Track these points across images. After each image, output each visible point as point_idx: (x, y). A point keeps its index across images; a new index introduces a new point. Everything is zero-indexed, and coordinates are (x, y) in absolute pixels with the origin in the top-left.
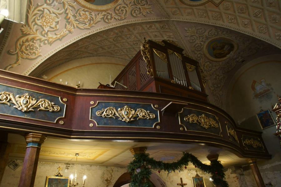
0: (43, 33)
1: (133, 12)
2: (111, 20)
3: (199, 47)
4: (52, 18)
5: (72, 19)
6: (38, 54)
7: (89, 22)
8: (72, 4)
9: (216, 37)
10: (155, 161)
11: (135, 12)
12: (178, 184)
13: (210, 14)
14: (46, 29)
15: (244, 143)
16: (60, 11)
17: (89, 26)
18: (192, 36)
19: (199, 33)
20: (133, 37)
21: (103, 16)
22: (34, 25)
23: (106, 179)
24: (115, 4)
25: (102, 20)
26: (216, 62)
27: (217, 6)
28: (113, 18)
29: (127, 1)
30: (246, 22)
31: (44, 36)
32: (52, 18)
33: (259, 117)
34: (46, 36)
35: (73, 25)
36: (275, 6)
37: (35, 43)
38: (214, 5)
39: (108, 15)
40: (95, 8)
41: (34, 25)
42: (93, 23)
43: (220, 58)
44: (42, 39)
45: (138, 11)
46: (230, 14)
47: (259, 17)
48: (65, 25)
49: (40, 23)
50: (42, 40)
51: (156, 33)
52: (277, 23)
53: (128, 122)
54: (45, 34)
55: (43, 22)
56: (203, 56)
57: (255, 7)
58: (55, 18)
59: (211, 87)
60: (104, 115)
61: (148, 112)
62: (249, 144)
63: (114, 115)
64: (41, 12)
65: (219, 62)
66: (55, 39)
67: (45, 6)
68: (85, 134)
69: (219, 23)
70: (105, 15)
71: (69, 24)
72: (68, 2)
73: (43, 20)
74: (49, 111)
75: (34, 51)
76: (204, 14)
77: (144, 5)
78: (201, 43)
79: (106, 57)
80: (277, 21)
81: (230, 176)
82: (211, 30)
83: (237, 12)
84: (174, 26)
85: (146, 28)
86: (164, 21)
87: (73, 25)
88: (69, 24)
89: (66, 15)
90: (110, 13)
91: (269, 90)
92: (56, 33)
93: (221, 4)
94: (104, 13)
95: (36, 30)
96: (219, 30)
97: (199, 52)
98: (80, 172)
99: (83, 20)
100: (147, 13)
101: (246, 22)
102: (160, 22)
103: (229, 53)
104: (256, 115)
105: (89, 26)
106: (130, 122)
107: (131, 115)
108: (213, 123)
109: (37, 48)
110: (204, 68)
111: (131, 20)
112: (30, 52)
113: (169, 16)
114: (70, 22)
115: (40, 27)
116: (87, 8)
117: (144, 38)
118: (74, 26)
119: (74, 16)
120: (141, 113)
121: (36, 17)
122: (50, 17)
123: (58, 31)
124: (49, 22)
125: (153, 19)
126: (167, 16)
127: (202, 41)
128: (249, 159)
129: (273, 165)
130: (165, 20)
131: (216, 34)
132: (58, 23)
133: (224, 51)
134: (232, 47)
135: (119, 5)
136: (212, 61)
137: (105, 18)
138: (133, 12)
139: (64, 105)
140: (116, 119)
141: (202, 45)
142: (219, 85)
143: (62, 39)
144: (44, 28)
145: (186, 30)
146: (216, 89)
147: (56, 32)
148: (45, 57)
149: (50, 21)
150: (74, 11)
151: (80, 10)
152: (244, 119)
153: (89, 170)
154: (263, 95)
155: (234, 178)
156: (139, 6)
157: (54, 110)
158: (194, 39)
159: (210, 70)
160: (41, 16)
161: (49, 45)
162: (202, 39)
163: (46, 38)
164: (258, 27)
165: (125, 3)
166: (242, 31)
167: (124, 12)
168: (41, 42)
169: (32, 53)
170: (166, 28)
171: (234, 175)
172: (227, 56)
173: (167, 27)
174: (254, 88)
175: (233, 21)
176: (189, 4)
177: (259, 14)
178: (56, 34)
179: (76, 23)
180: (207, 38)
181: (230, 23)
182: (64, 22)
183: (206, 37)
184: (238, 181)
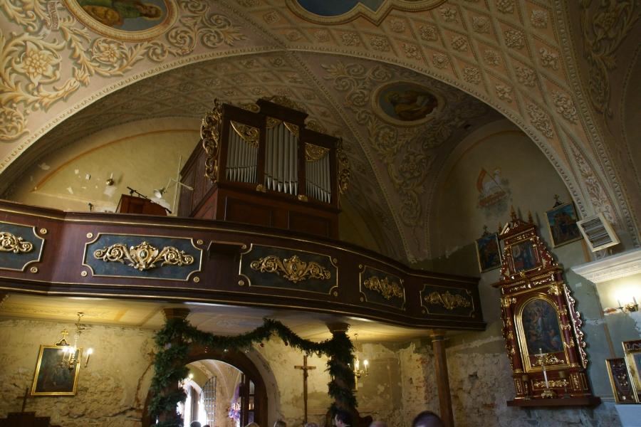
0: (31, 87)
1: (205, 39)
2: (163, 56)
4: (45, 59)
5: (84, 57)
6: (21, 130)
7: (119, 62)
8: (80, 30)
9: (391, 82)
10: (200, 332)
11: (209, 39)
12: (295, 367)
13: (365, 39)
14: (36, 80)
15: (423, 300)
16: (58, 44)
17: (119, 70)
18: (340, 79)
20: (219, 82)
21: (146, 49)
22: (10, 74)
23: (150, 351)
24: (165, 27)
25: (146, 56)
26: (404, 127)
27: (378, 24)
28: (167, 52)
30: (441, 57)
31: (33, 95)
32: (45, 59)
33: (479, 247)
34: (36, 93)
35: (88, 69)
36: (487, 33)
37: (15, 108)
39: (156, 47)
40: (126, 36)
41: (10, 74)
42: (128, 63)
43: (412, 120)
44: (28, 99)
46: (407, 41)
47: (463, 51)
48: (71, 71)
49: (22, 68)
50: (29, 101)
51: (265, 74)
52: (496, 65)
53: (144, 270)
54: (33, 89)
55: (27, 67)
56: (373, 117)
58: (50, 57)
59: (396, 178)
60: (106, 258)
61: (183, 252)
62: (437, 302)
63: (122, 258)
64: (22, 49)
65: (411, 127)
66: (54, 98)
67: (26, 36)
68: (71, 289)
69: (388, 58)
70: (148, 48)
71: (80, 69)
72: (71, 28)
73: (28, 63)
74: (12, 251)
75: (15, 124)
76: (355, 40)
77: (224, 26)
78: (362, 93)
79: (176, 118)
80: (496, 62)
81: (413, 358)
83: (419, 37)
85: (241, 67)
86: (275, 52)
87: (88, 69)
88: (80, 69)
89: (70, 51)
90: (159, 42)
91: (503, 193)
92: (57, 88)
93: (384, 22)
94: (146, 44)
95: (16, 84)
97: (362, 109)
98: (102, 338)
99: (107, 59)
101: (441, 57)
104: (476, 242)
105: (119, 70)
106: (148, 271)
107: (151, 259)
108: (315, 270)
109: (21, 118)
110: (377, 140)
111: (203, 55)
112: (6, 127)
113: (282, 43)
114: (80, 65)
115: (22, 77)
116: (110, 36)
117: (215, 100)
118: (89, 71)
119: (87, 52)
120: (169, 254)
121: (13, 58)
122: (41, 57)
123: (59, 82)
124: (40, 66)
125: (250, 49)
127: (364, 88)
128: (431, 331)
129: (486, 341)
130: (277, 50)
131: (390, 76)
132: (57, 66)
134: (432, 103)
135: (173, 29)
136: (395, 125)
137: (150, 54)
138: (205, 39)
139: (42, 240)
140: (125, 263)
141: (365, 96)
142: (416, 174)
143: (67, 97)
144: (32, 77)
145: (326, 69)
146: (408, 182)
147: (56, 85)
148: (36, 136)
149: (40, 64)
150: (86, 43)
151: (98, 40)
152: (456, 249)
153: (120, 336)
154: (494, 201)
155: (417, 360)
156: (214, 29)
157: (21, 250)
158: (347, 84)
159: (393, 144)
160: (22, 55)
161: (43, 112)
163: (36, 98)
164: (464, 70)
165: (184, 25)
167: (188, 40)
168: (26, 105)
169: (10, 129)
171: (417, 356)
173: (284, 62)
174: (480, 186)
175: (414, 54)
177: (462, 45)
178: (55, 89)
179: (93, 66)
181: (408, 57)
182: (71, 64)
183: (371, 81)
184: (423, 367)
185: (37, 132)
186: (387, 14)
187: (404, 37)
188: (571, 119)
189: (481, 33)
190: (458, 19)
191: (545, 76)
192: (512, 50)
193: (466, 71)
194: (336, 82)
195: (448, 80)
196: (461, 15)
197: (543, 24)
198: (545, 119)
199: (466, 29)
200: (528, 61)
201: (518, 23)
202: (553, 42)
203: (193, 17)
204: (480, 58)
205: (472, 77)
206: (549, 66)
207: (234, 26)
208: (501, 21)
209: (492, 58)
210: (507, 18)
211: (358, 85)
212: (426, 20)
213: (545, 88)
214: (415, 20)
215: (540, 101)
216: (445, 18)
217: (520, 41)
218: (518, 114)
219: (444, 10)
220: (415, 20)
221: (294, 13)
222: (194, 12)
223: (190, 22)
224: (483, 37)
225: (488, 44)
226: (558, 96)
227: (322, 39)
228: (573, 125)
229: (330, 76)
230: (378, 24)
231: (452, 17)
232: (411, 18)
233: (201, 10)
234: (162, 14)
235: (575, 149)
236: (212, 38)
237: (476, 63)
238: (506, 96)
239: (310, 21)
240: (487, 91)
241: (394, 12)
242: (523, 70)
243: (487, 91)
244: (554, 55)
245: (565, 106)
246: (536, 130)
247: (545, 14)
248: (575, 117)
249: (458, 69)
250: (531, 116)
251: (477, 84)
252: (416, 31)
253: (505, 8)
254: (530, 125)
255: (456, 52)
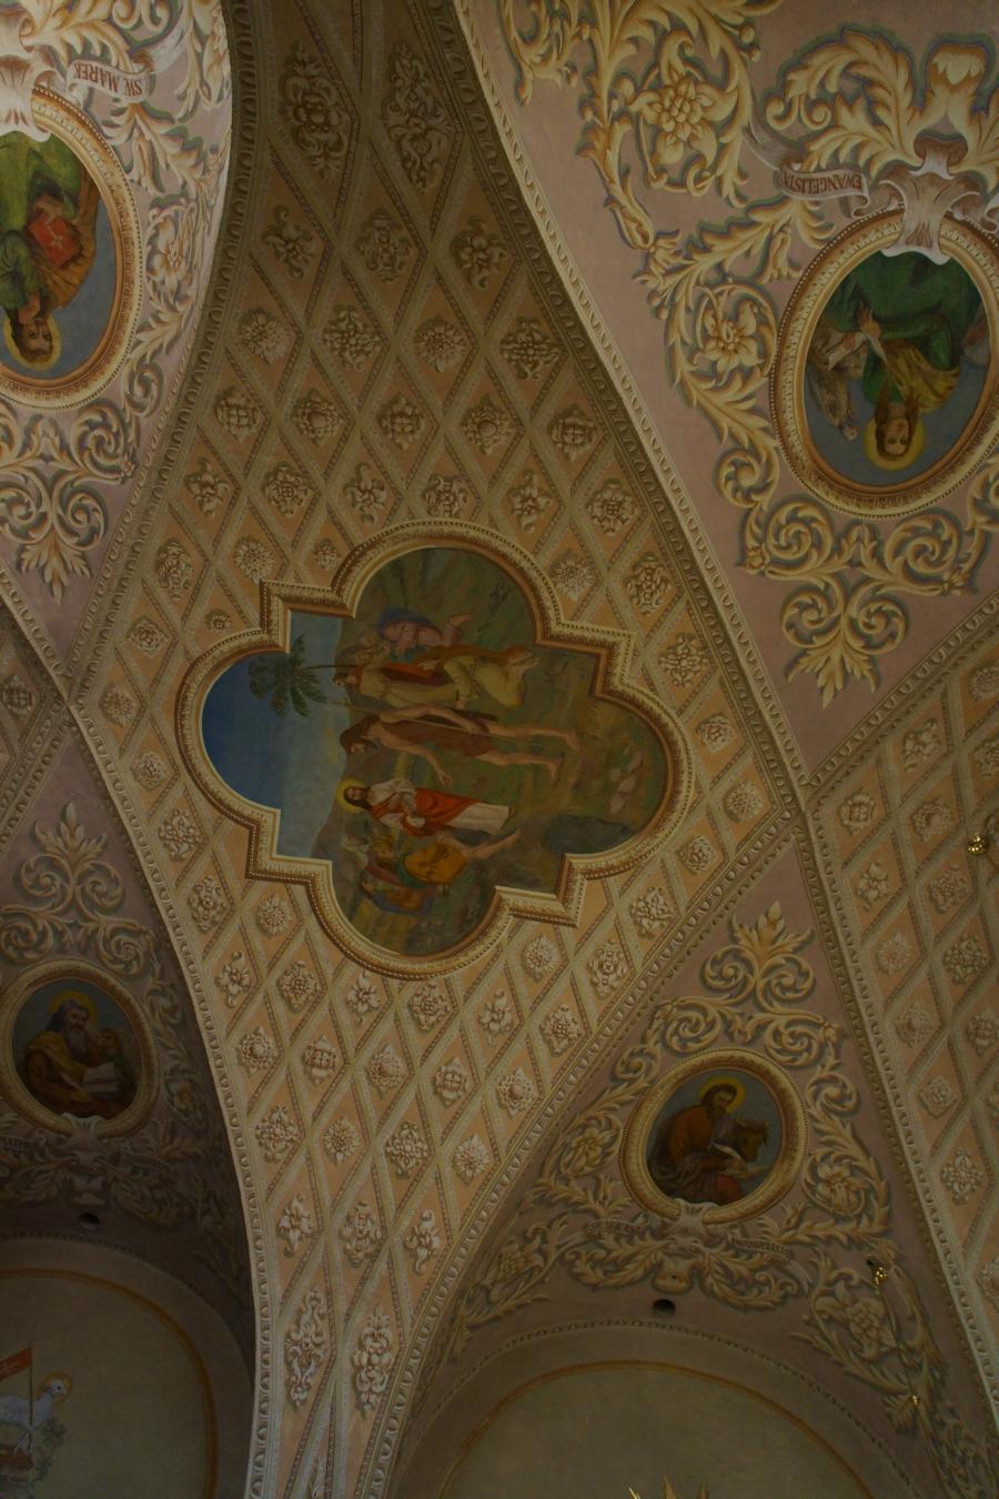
3: (21, 943)
13: (201, 867)
18: (52, 864)
19: (88, 887)
27: (253, 873)
29: (44, 439)
38: (248, 860)
43: (34, 1092)
45: (28, 515)
47: (312, 1078)
52: (335, 1161)
57: (336, 1026)
69: (187, 941)
76: (185, 847)
77: (71, 532)
78: (44, 934)
80: (340, 1157)
82: (137, 934)
84: (47, 744)
86: (49, 679)
91: (24, 1462)
96: (157, 968)
100: (42, 570)
102: (31, 661)
103: (83, 1111)
126: (79, 680)
127: (59, 934)
130: (57, 681)
131: (134, 970)
133: (80, 1080)
156: (51, 509)
158: (48, 888)
162: (69, 925)
165: (29, 431)
166: (218, 1062)
170: (15, 710)
172: (65, 1114)
175: (234, 989)
176: (186, 747)
177: (320, 1067)
180: (87, 947)
181: (217, 980)
183: (91, 937)
185: (527, 164)
186: (288, 880)
187: (257, 942)
188: (364, 1398)
189: (371, 1083)
190: (367, 1021)
191: (391, 1266)
192: (386, 1165)
193: (275, 1117)
194: (38, 862)
195: (228, 1096)
196: (377, 1021)
197: (469, 1173)
198: (319, 1352)
199: (357, 1050)
200: (390, 1212)
201: (437, 1130)
202: (455, 1219)
203: (64, 448)
204: (325, 1119)
205: (274, 1137)
206: (412, 1253)
207: (83, 557)
208: (419, 1100)
209: (340, 1142)
210: (432, 1103)
211: (63, 913)
212: (324, 965)
213: (371, 1287)
214: (308, 942)
215: (342, 1306)
216: (352, 996)
217: (412, 1163)
218: (279, 1290)
219: (365, 983)
220: (308, 942)
221: (183, 683)
222: (82, 448)
223: (45, 442)
224: (366, 1092)
225: (361, 1113)
226: (378, 1328)
227: (145, 774)
228: (358, 1413)
229: (48, 838)
230: (253, 873)
231: (362, 1008)
232: (307, 932)
233: (95, 464)
234: (37, 366)
235: (320, 1477)
236: (21, 511)
237: (308, 1118)
238: (294, 1235)
239: (178, 727)
240: (271, 1190)
241: (299, 890)
242: (368, 1216)
243: (271, 1190)
244: (437, 1243)
245: (375, 1359)
246: (282, 1360)
247: (486, 1161)
248: (373, 1399)
249: (269, 1097)
250: (298, 1323)
251: (267, 1159)
252: (287, 958)
253: (444, 1087)
254: (281, 1339)
255: (298, 1066)
